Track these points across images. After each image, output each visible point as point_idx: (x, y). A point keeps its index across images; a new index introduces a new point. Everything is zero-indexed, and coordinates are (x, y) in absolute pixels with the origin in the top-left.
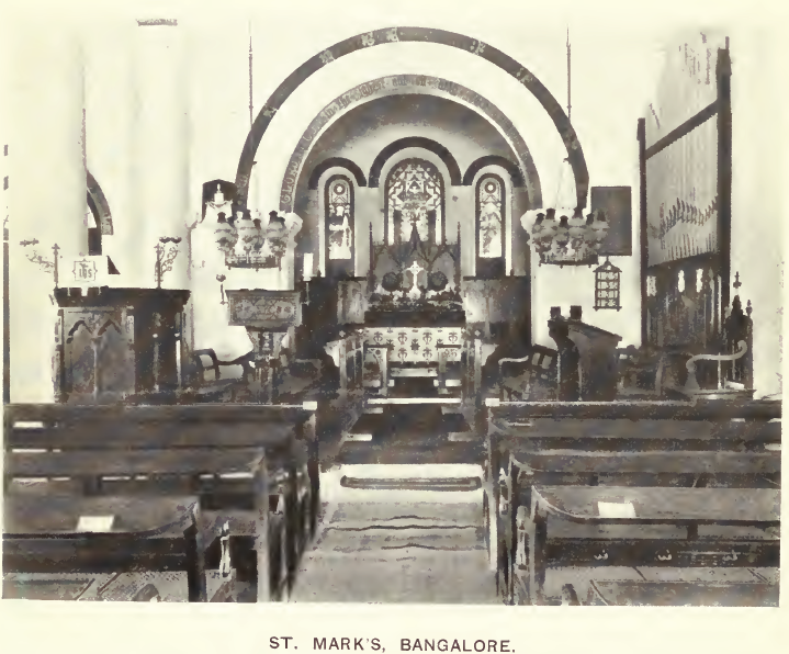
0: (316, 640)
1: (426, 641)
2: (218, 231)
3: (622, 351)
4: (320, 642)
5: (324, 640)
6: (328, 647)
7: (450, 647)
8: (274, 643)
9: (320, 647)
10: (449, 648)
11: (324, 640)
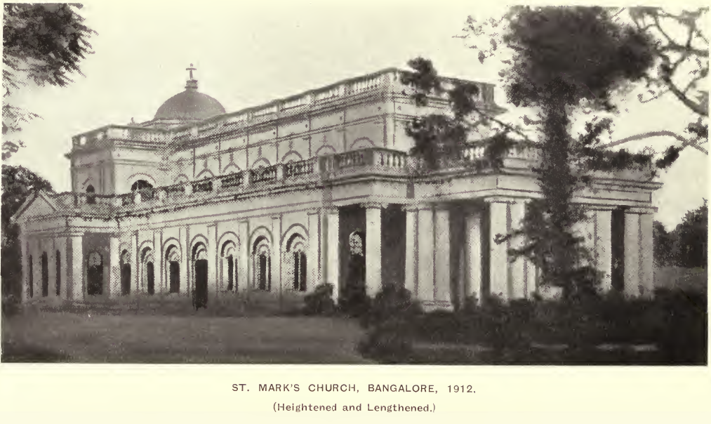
0: (260, 385)
1: (384, 386)
2: (83, 57)
3: (571, 203)
4: (263, 386)
5: (265, 385)
6: (268, 389)
7: (398, 389)
8: (235, 388)
9: (263, 390)
10: (398, 390)
11: (265, 385)
